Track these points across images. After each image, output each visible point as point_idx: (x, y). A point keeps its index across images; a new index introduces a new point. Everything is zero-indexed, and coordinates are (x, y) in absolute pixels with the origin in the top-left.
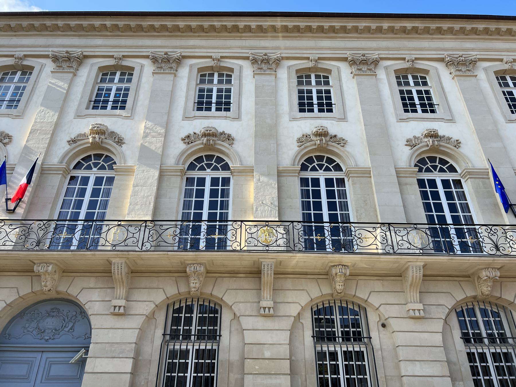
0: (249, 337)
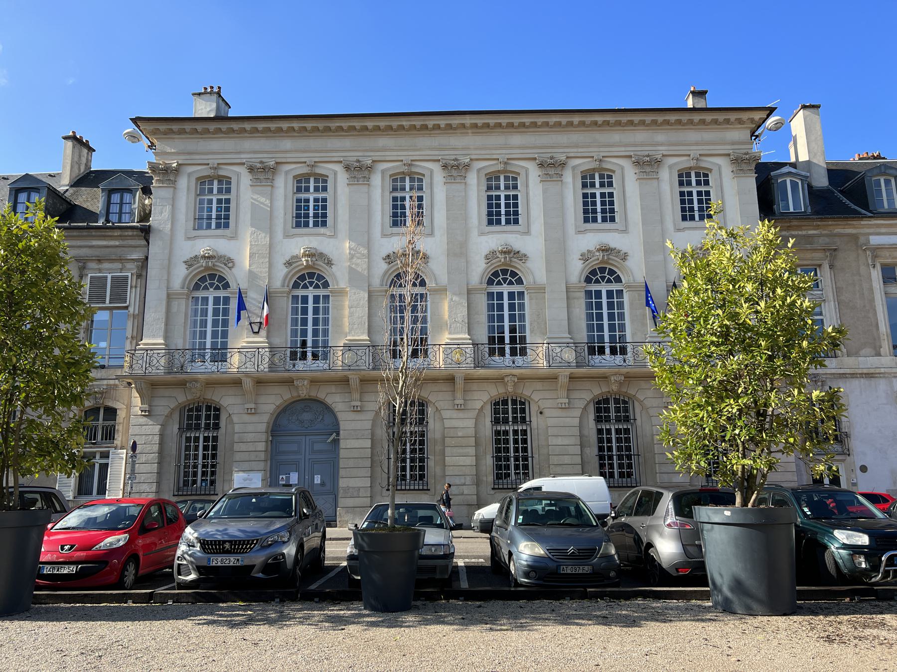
0: (448, 424)
